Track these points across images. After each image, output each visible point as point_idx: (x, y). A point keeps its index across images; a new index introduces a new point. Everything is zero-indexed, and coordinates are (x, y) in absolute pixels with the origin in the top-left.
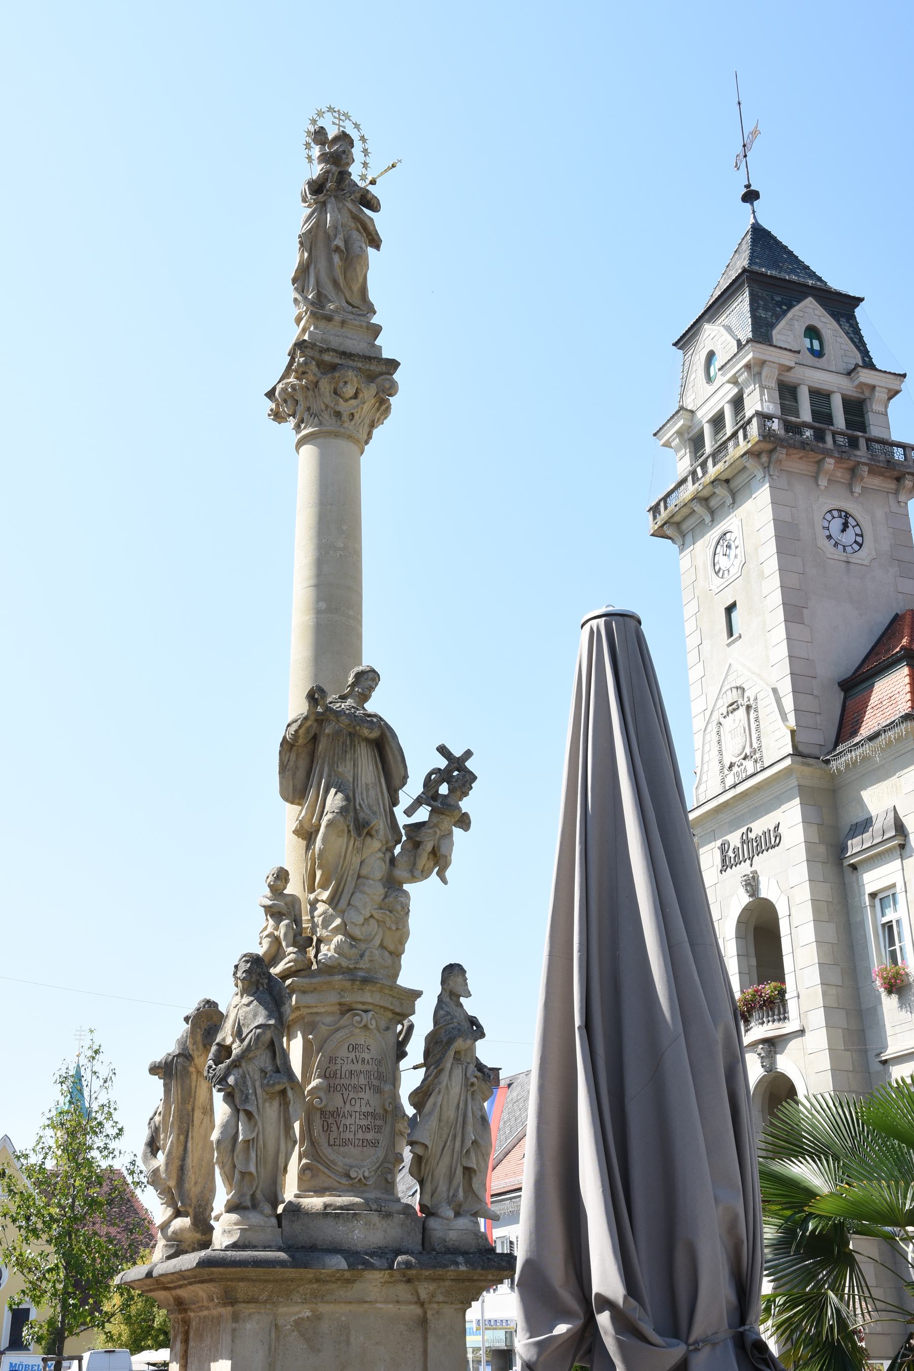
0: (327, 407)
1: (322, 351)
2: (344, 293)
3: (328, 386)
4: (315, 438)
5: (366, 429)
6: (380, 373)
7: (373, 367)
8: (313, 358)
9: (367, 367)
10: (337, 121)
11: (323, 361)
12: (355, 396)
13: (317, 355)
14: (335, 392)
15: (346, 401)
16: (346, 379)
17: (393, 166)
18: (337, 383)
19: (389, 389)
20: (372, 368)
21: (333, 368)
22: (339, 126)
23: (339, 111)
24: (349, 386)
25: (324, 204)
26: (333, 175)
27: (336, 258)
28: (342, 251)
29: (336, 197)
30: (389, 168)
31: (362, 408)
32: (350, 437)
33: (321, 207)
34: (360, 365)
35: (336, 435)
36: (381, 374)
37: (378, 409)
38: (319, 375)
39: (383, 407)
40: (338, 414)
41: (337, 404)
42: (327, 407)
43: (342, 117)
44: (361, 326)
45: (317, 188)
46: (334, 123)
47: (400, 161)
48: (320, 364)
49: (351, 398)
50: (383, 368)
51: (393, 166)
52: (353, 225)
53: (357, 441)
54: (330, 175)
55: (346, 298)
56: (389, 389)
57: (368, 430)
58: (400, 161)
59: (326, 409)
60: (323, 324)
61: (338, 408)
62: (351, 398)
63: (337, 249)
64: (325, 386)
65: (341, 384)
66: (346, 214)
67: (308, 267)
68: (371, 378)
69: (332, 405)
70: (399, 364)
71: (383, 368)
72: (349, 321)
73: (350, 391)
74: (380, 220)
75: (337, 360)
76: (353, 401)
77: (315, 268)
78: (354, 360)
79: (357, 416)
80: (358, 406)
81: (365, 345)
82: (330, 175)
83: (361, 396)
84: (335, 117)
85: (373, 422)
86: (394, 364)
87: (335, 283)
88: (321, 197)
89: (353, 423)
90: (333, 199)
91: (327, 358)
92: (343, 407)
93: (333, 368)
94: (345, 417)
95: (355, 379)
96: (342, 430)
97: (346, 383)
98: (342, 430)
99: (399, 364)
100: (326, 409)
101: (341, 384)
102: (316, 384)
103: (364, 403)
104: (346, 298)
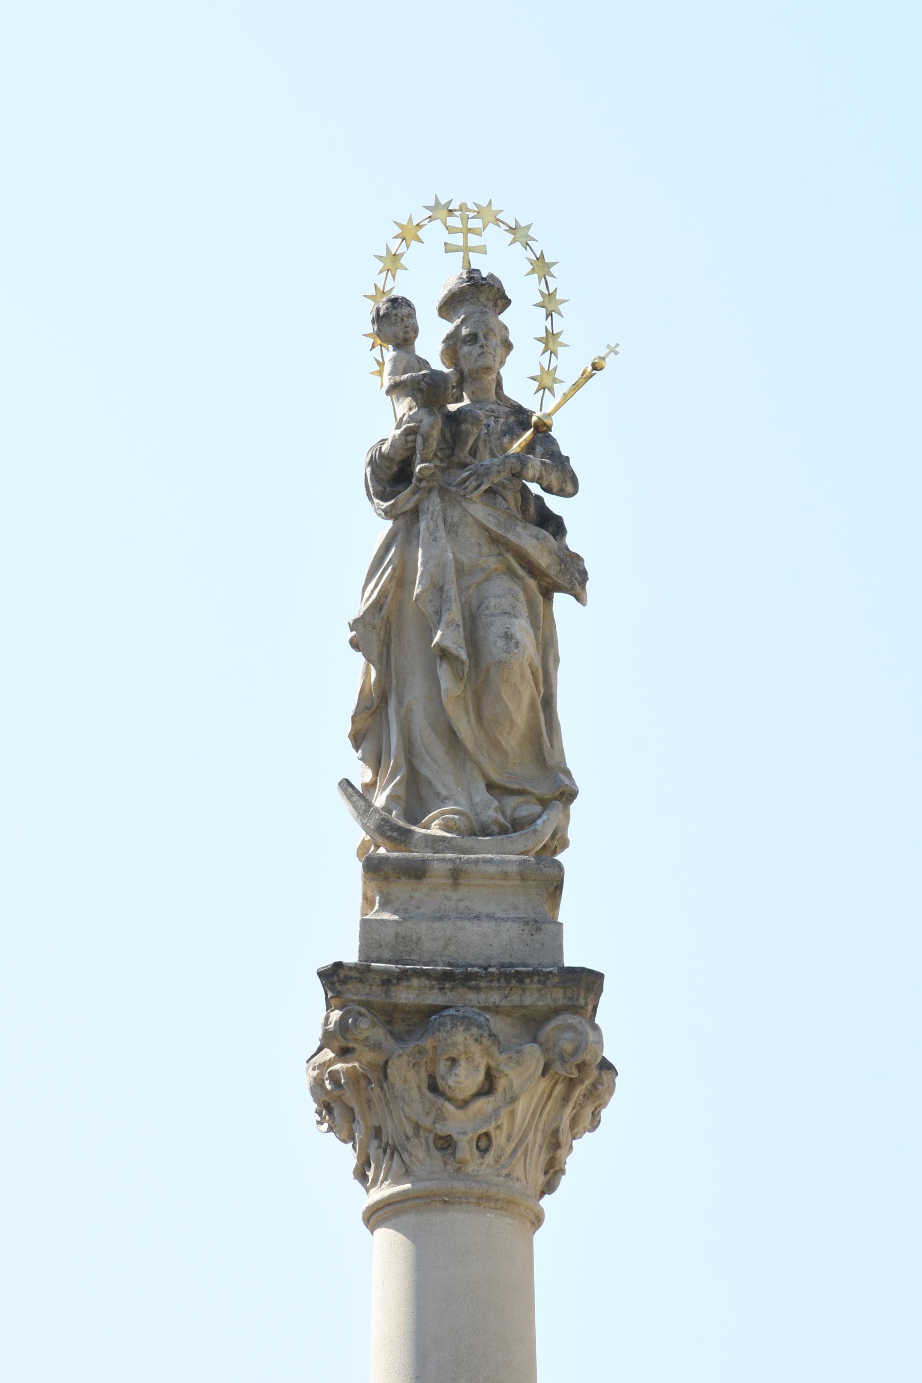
0: (417, 1127)
1: (388, 981)
2: (478, 764)
3: (411, 1075)
4: (398, 1213)
5: (537, 1159)
6: (552, 1005)
7: (532, 998)
8: (367, 1005)
9: (515, 999)
10: (457, 239)
11: (396, 1007)
12: (488, 1088)
13: (377, 995)
14: (434, 1087)
15: (464, 1104)
16: (454, 1053)
17: (596, 367)
18: (434, 1062)
19: (576, 1052)
20: (528, 1001)
21: (426, 1017)
22: (466, 249)
23: (463, 208)
24: (462, 1070)
25: (415, 513)
26: (425, 439)
27: (444, 674)
28: (457, 658)
29: (443, 491)
30: (586, 377)
31: (513, 1113)
32: (483, 1200)
33: (406, 525)
34: (495, 998)
35: (447, 1200)
36: (557, 1011)
37: (566, 1099)
38: (389, 1043)
39: (584, 1082)
40: (446, 1144)
41: (440, 1117)
42: (417, 1127)
43: (474, 224)
44: (506, 875)
45: (392, 475)
46: (449, 248)
47: (613, 350)
48: (389, 1016)
49: (479, 1094)
50: (558, 996)
51: (596, 367)
52: (492, 563)
53: (505, 1204)
54: (419, 439)
55: (485, 776)
56: (576, 1052)
57: (544, 1158)
58: (613, 350)
59: (417, 1135)
60: (402, 889)
61: (442, 1129)
62: (479, 1094)
63: (444, 653)
64: (405, 1075)
65: (443, 1067)
66: (470, 534)
67: (384, 698)
68: (533, 1023)
69: (427, 1122)
70: (599, 977)
71: (558, 996)
72: (472, 868)
73: (466, 1080)
74: (582, 520)
75: (434, 998)
76: (484, 1105)
77: (400, 703)
78: (477, 989)
79: (500, 1138)
80: (496, 1112)
81: (516, 928)
82: (419, 439)
83: (501, 1084)
84: (451, 230)
85: (555, 1133)
86: (589, 982)
87: (453, 740)
88: (406, 498)
89: (490, 1158)
90: (435, 498)
91: (405, 996)
92: (459, 1123)
93: (426, 1017)
94: (465, 1149)
95: (475, 1048)
96: (459, 1186)
97: (454, 1061)
98: (459, 1186)
99: (599, 977)
100: (417, 1135)
101: (443, 1067)
102: (384, 1069)
103: (513, 1100)
104: (485, 776)
